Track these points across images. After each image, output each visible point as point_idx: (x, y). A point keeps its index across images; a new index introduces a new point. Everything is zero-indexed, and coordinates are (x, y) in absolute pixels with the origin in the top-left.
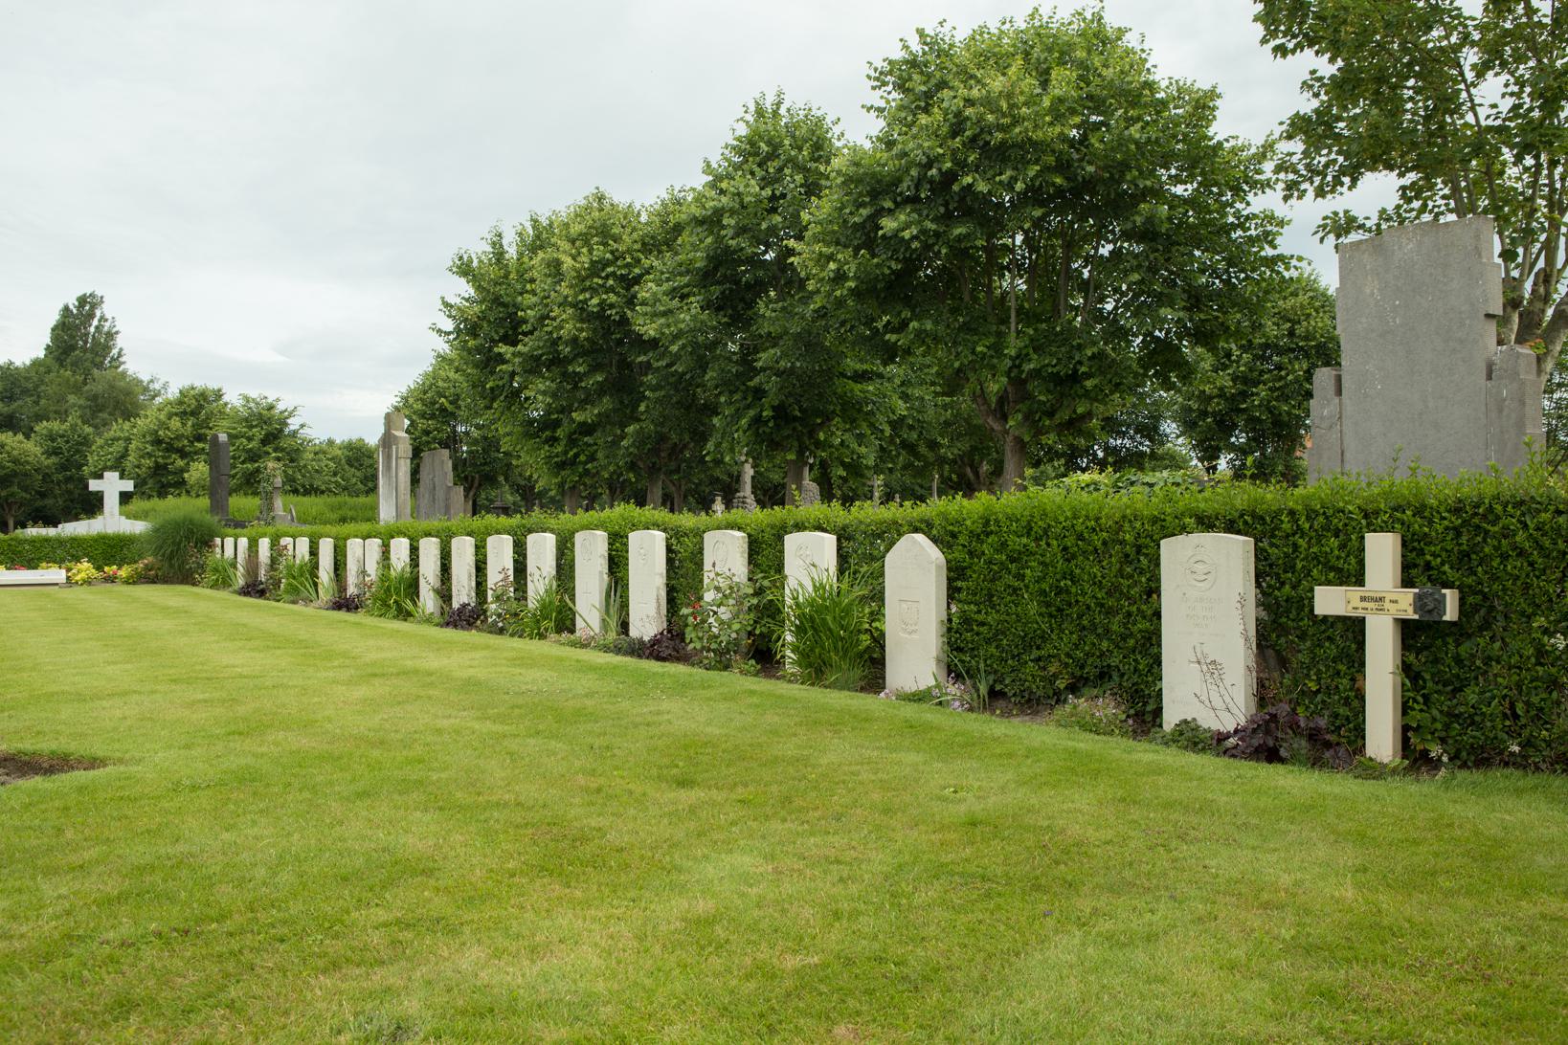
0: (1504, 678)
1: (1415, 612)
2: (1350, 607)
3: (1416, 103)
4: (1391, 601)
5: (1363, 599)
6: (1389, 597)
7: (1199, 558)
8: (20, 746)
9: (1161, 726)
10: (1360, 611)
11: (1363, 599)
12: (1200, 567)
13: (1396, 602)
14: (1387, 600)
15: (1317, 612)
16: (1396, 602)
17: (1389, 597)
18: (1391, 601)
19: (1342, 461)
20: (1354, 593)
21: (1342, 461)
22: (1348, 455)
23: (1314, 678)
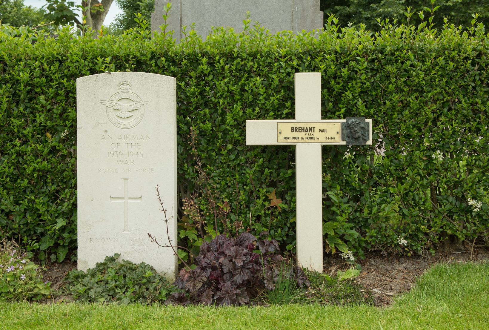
0: (394, 187)
1: (343, 140)
2: (281, 138)
3: (18, 268)
4: (321, 131)
5: (294, 130)
6: (318, 127)
7: (125, 96)
8: (196, 312)
9: (75, 263)
10: (291, 140)
11: (294, 130)
12: (125, 105)
13: (325, 131)
14: (317, 130)
15: (248, 144)
16: (325, 131)
17: (318, 127)
18: (321, 131)
19: (181, 24)
20: (285, 125)
21: (181, 24)
22: (185, 21)
23: (227, 200)
